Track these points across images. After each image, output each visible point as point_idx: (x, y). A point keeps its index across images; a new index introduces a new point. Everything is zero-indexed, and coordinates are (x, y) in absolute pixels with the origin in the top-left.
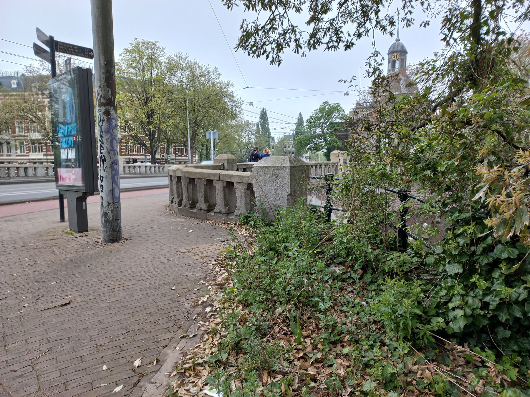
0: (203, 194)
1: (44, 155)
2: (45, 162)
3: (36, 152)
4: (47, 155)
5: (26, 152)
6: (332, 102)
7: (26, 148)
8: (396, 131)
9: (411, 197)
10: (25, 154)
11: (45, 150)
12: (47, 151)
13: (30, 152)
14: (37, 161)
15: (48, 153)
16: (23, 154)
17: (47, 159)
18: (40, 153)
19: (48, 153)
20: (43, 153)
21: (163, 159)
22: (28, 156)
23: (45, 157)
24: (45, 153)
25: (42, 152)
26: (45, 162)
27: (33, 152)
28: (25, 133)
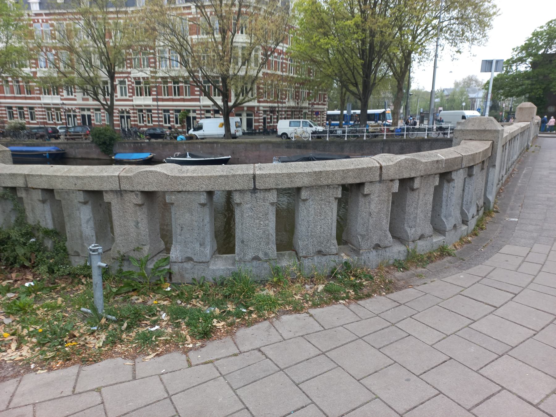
0: (301, 163)
1: (154, 100)
2: (198, 110)
3: (141, 95)
4: (157, 100)
5: (128, 94)
6: (495, 22)
7: (129, 89)
8: (208, 56)
9: (120, 188)
10: (127, 98)
11: (155, 93)
12: (157, 95)
13: (134, 95)
14: (143, 108)
15: (159, 97)
16: (124, 97)
17: (158, 106)
18: (148, 97)
19: (159, 97)
20: (151, 97)
21: (297, 108)
22: (132, 100)
23: (155, 103)
24: (155, 97)
25: (150, 95)
26: (198, 110)
27: (146, 95)
28: (127, 67)
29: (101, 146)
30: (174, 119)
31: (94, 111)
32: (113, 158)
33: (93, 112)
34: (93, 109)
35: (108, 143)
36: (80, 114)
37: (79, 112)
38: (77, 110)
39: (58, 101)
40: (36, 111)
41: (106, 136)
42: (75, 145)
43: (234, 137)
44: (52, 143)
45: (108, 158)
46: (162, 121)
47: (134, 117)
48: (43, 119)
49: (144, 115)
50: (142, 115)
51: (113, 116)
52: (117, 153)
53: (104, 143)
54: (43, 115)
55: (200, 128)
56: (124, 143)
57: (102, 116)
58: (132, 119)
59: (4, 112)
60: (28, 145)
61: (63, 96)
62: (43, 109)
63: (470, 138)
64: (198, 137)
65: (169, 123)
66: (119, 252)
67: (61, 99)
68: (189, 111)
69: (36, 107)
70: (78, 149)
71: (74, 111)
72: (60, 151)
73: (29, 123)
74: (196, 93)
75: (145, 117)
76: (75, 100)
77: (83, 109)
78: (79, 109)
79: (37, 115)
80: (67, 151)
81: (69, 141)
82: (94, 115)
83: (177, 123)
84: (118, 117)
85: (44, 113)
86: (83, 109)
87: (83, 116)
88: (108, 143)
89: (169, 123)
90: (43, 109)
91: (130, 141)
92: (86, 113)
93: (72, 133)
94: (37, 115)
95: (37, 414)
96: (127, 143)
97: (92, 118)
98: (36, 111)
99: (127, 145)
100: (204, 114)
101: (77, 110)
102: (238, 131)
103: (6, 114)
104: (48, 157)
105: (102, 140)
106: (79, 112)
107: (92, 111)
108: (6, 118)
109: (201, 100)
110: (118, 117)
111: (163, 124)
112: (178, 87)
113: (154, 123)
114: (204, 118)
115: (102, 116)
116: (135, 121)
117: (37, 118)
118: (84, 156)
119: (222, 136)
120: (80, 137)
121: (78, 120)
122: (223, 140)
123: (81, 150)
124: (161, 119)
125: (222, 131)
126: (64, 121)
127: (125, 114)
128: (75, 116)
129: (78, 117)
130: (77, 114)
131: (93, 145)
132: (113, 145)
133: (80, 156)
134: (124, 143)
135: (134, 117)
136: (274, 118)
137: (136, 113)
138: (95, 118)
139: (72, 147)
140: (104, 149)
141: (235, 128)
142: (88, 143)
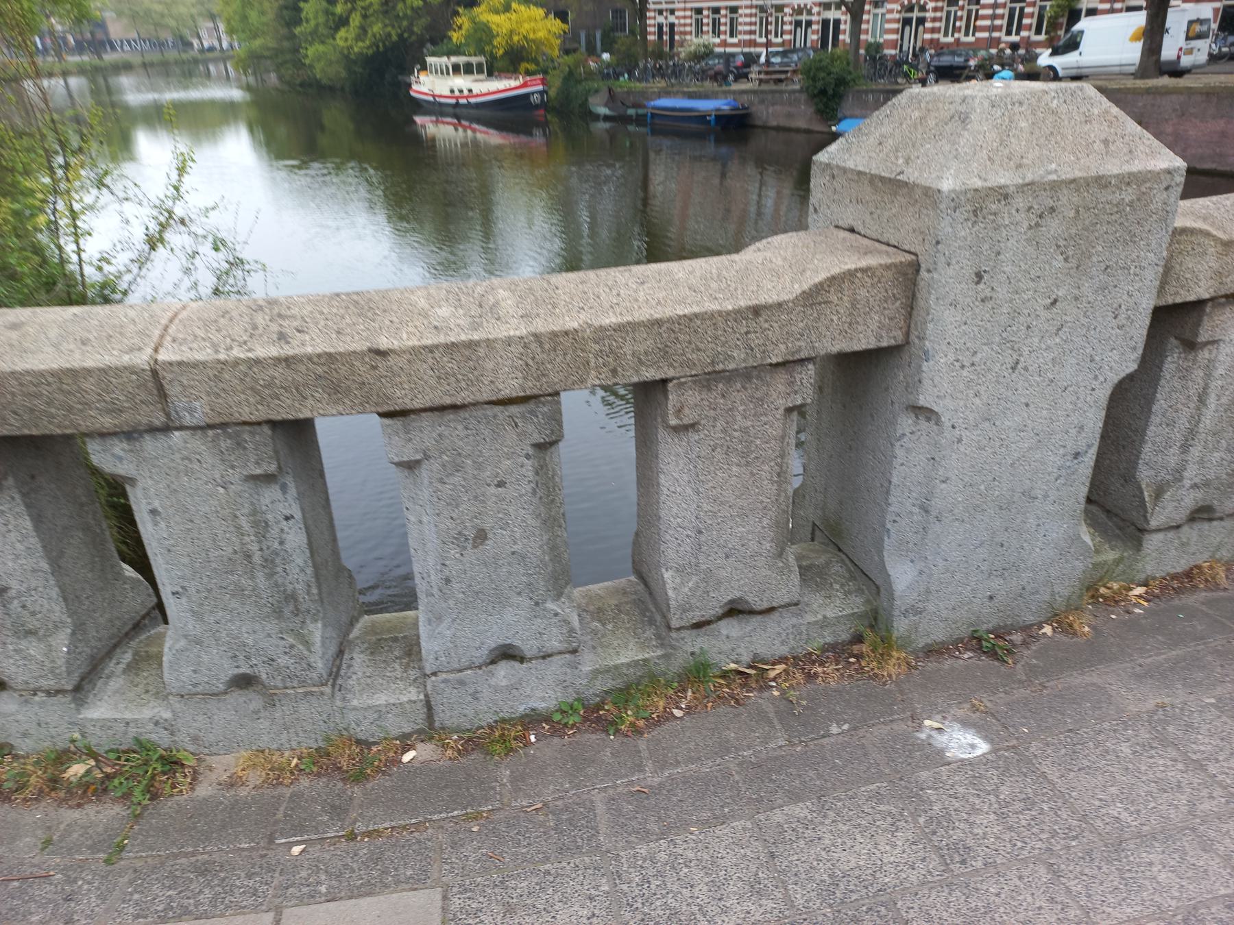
29: (816, 100)
30: (1034, 21)
32: (834, 128)
35: (830, 92)
38: (815, 10)
40: (741, 16)
41: (829, 74)
42: (770, 97)
43: (1176, 71)
44: (730, 92)
45: (825, 129)
46: (999, 28)
47: (934, 20)
48: (751, 32)
49: (959, 13)
50: (977, 11)
51: (861, 21)
52: (845, 117)
53: (823, 92)
54: (751, 24)
56: (866, 92)
58: (928, 25)
59: (688, 21)
60: (691, 96)
63: (848, 221)
64: (1061, 73)
65: (1018, 33)
69: (741, 7)
70: (773, 104)
71: (810, 12)
72: (738, 109)
73: (724, 44)
75: (961, 18)
79: (741, 24)
80: (753, 109)
81: (765, 87)
83: (1038, 32)
84: (898, 21)
85: (753, 19)
87: (825, 23)
88: (830, 92)
89: (1018, 33)
90: (688, 13)
91: (881, 87)
93: (777, 68)
94: (741, 24)
95: (1231, 512)
96: (872, 91)
97: (842, 27)
98: (741, 16)
99: (870, 97)
101: (815, 10)
102: (1190, 52)
104: (713, 123)
105: (820, 85)
106: (819, 14)
108: (691, 33)
110: (898, 21)
111: (1001, 35)
114: (1120, 11)
116: (933, 30)
117: (740, 33)
118: (783, 122)
119: (1132, 69)
120: (783, 76)
121: (813, 32)
122: (1131, 83)
123: (778, 108)
124: (998, 22)
125: (1132, 53)
126: (787, 37)
127: (915, 14)
128: (809, 23)
129: (815, 27)
130: (814, 18)
131: (803, 97)
132: (841, 97)
133: (774, 123)
134: (866, 92)
135: (934, 20)
136: (1032, 15)
137: (941, 9)
139: (762, 102)
140: (821, 106)
141: (1181, 41)
142: (794, 92)
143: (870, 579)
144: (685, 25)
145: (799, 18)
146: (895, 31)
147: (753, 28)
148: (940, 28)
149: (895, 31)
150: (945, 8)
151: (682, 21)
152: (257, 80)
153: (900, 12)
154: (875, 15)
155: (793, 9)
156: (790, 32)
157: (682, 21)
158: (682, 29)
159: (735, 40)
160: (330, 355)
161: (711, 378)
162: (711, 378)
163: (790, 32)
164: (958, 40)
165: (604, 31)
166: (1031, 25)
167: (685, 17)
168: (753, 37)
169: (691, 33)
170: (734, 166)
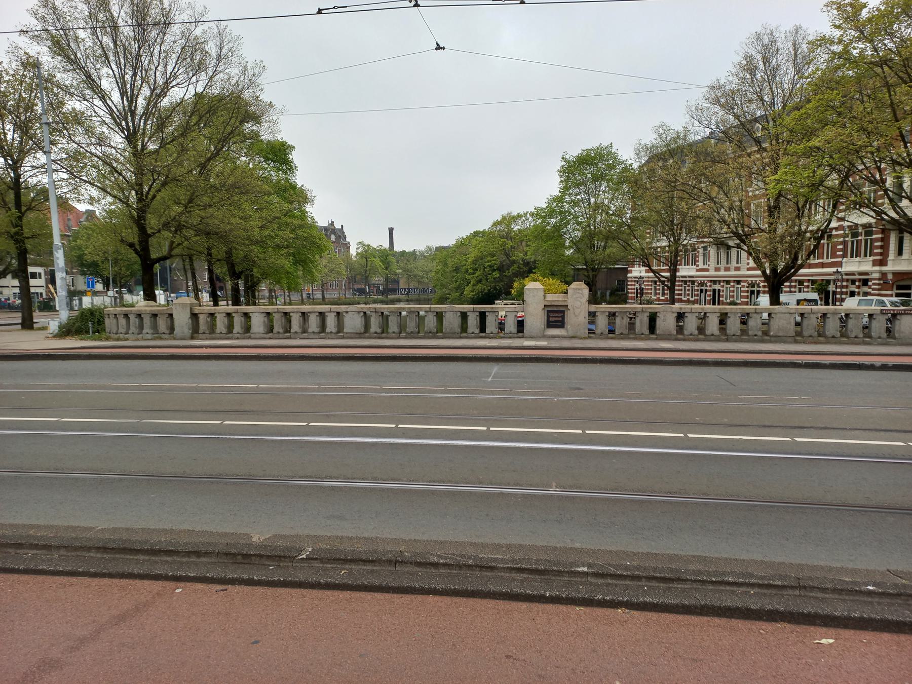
20: (872, 258)
31: (725, 284)
33: (723, 286)
34: (724, 281)
36: (712, 289)
37: (710, 286)
38: (709, 284)
39: (693, 273)
55: (57, 252)
57: (730, 291)
61: (698, 266)
62: (650, 283)
66: (282, 138)
67: (697, 271)
68: (828, 282)
71: (759, 286)
74: (838, 253)
76: (707, 270)
77: (715, 282)
78: (711, 281)
82: (725, 289)
84: (747, 292)
86: (715, 282)
87: (714, 290)
90: (650, 283)
92: (717, 287)
100: (847, 287)
101: (709, 284)
103: (651, 289)
106: (710, 286)
107: (732, 284)
109: (844, 264)
110: (747, 292)
112: (857, 241)
113: (742, 300)
115: (730, 291)
128: (706, 291)
138: (724, 293)
143: (869, 430)
144: (648, 289)
145: (702, 288)
146: (747, 297)
147: (680, 292)
148: (734, 295)
149: (747, 297)
150: (798, 286)
151: (647, 287)
152: (140, 306)
153: (748, 287)
154: (727, 288)
155: (699, 284)
156: (697, 295)
157: (647, 287)
158: (647, 291)
159: (663, 298)
160: (520, 545)
161: (161, 314)
162: (161, 314)
163: (697, 295)
164: (688, 299)
165: (612, 291)
166: (710, 295)
167: (648, 285)
168: (680, 297)
169: (651, 293)
170: (90, 306)
